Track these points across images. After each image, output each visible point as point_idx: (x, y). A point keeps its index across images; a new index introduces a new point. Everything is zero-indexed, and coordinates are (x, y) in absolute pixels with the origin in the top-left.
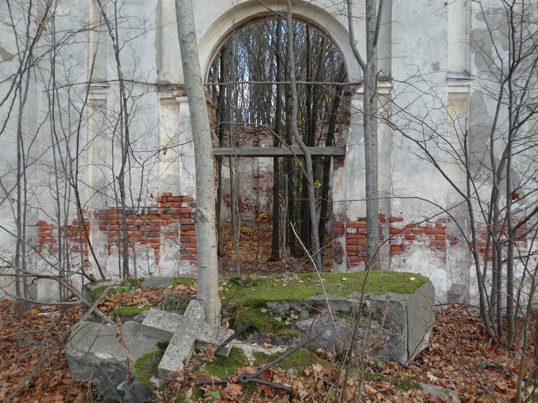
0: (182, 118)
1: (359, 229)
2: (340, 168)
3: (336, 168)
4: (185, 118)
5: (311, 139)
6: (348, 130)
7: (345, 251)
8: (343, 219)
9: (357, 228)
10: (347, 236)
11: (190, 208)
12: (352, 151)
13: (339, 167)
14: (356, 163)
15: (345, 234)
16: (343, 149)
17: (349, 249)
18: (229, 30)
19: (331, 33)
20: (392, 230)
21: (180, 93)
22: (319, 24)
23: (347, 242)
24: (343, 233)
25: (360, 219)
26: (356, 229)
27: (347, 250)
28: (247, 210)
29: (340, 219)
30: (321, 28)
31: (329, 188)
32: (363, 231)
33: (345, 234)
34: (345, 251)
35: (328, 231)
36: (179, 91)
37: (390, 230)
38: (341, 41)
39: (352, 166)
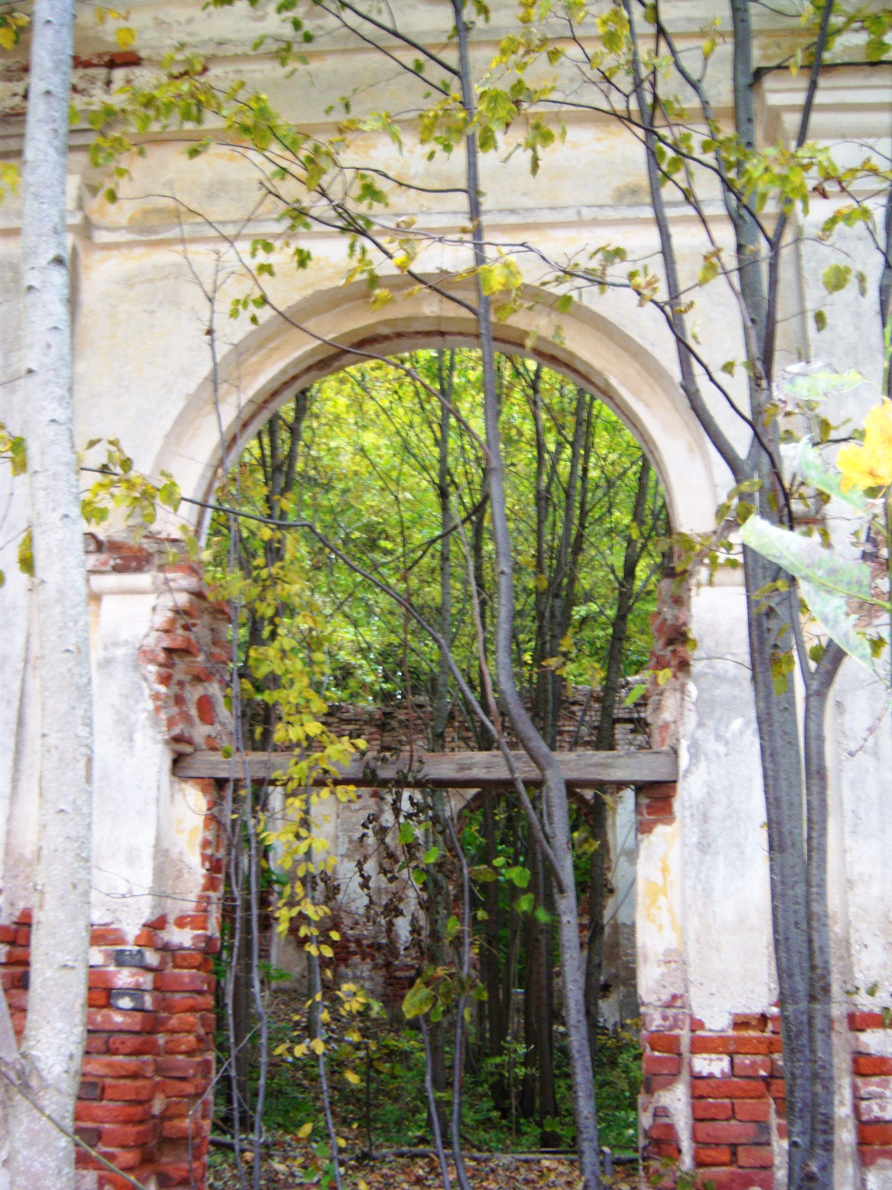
0: (106, 648)
1: (738, 1059)
2: (660, 830)
3: (643, 828)
4: (116, 644)
5: (580, 467)
6: (683, 690)
7: (686, 1144)
8: (676, 1018)
9: (731, 1054)
10: (693, 1087)
11: (112, 968)
12: (703, 765)
13: (655, 823)
14: (716, 811)
15: (685, 1076)
16: (103, 1048)
17: (701, 1136)
18: (283, 372)
19: (614, 382)
20: (862, 1060)
21: (105, 563)
22: (572, 355)
23: (694, 1109)
24: (679, 1072)
25: (741, 1023)
26: (726, 1060)
27: (694, 1138)
28: (357, 959)
29: (665, 1018)
30: (579, 366)
31: (611, 891)
32: (753, 1064)
33: (685, 1076)
34: (686, 1144)
35: (610, 1026)
36: (103, 557)
37: (855, 1061)
38: (648, 406)
39: (705, 819)
